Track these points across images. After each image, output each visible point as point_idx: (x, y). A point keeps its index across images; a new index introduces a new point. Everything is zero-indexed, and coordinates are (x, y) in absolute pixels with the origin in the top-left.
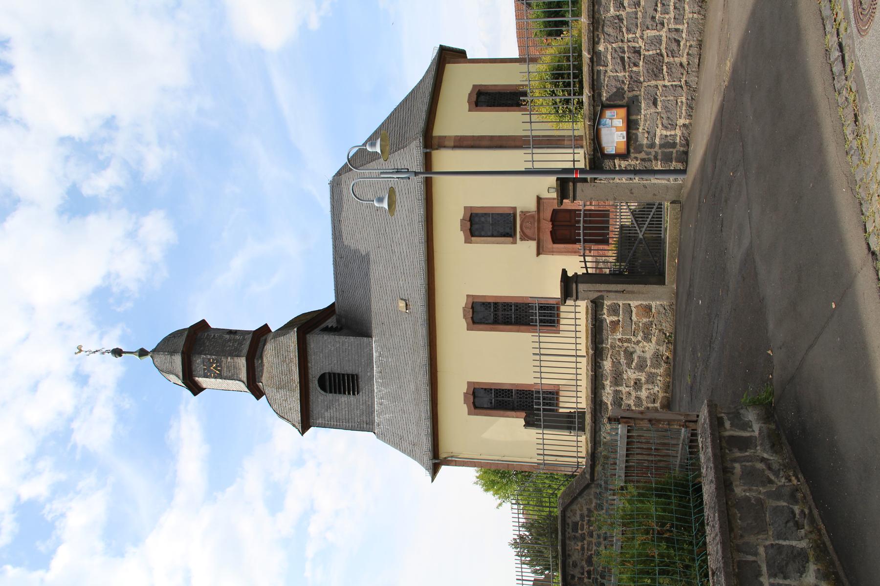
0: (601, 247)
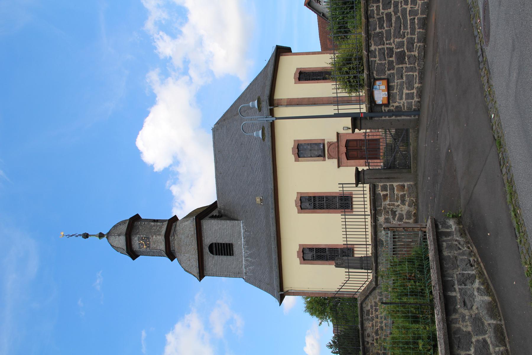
0: (376, 161)
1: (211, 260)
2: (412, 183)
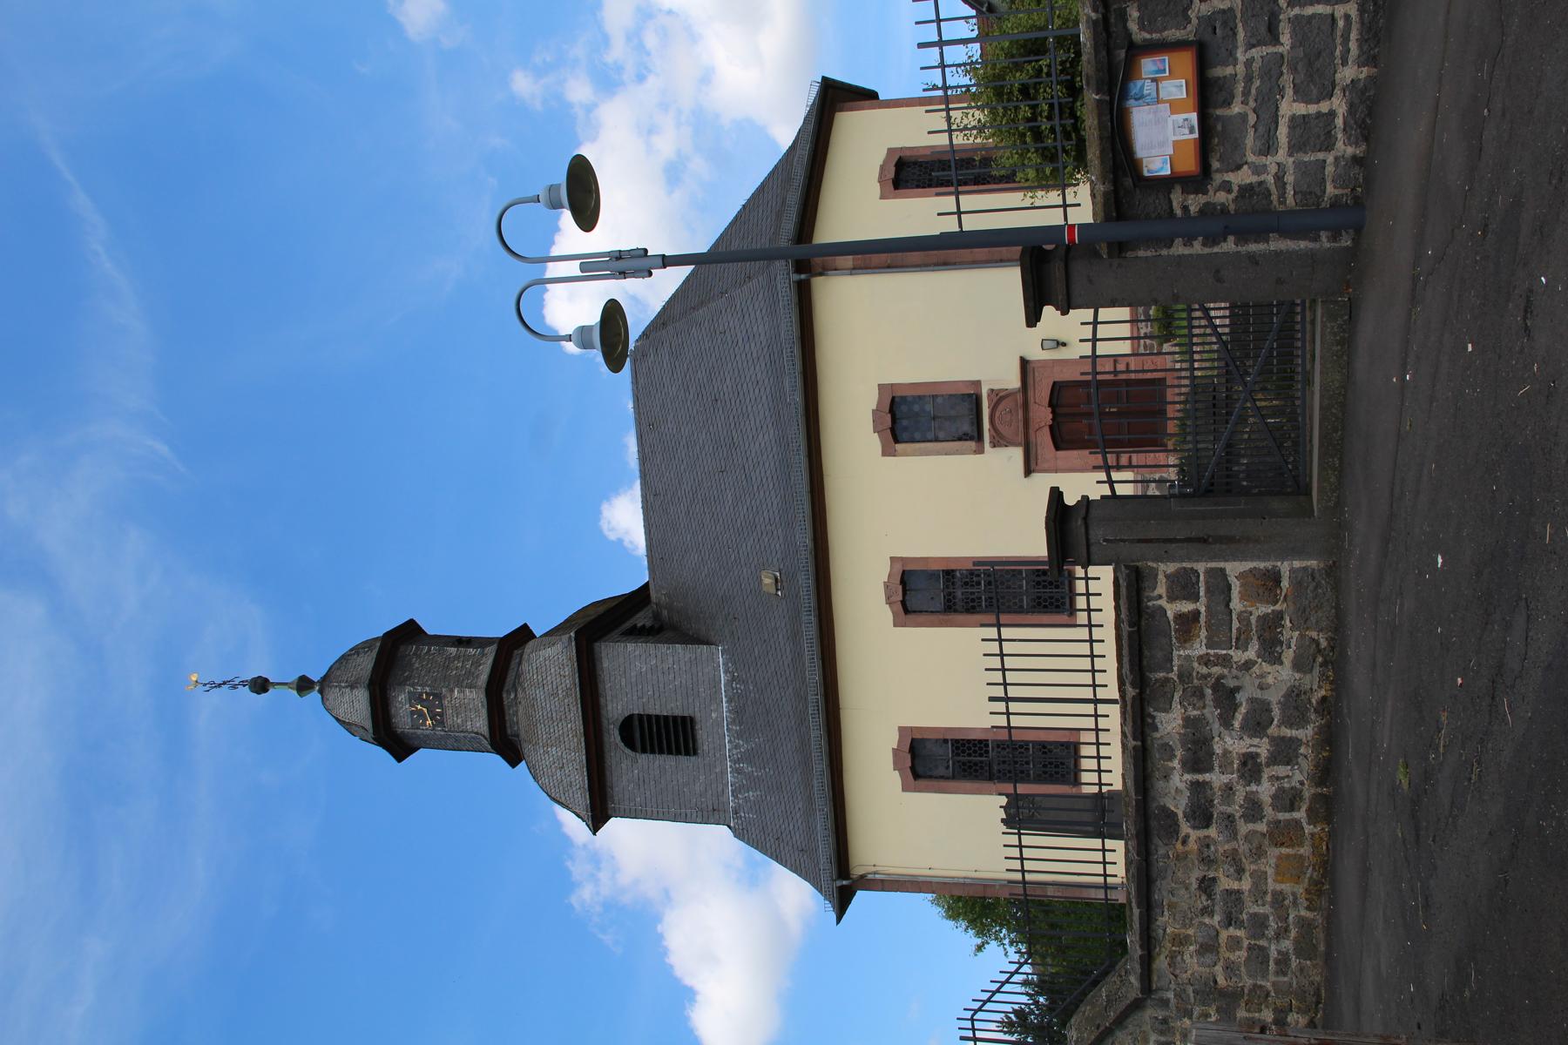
1: (628, 768)
2: (1313, 563)
